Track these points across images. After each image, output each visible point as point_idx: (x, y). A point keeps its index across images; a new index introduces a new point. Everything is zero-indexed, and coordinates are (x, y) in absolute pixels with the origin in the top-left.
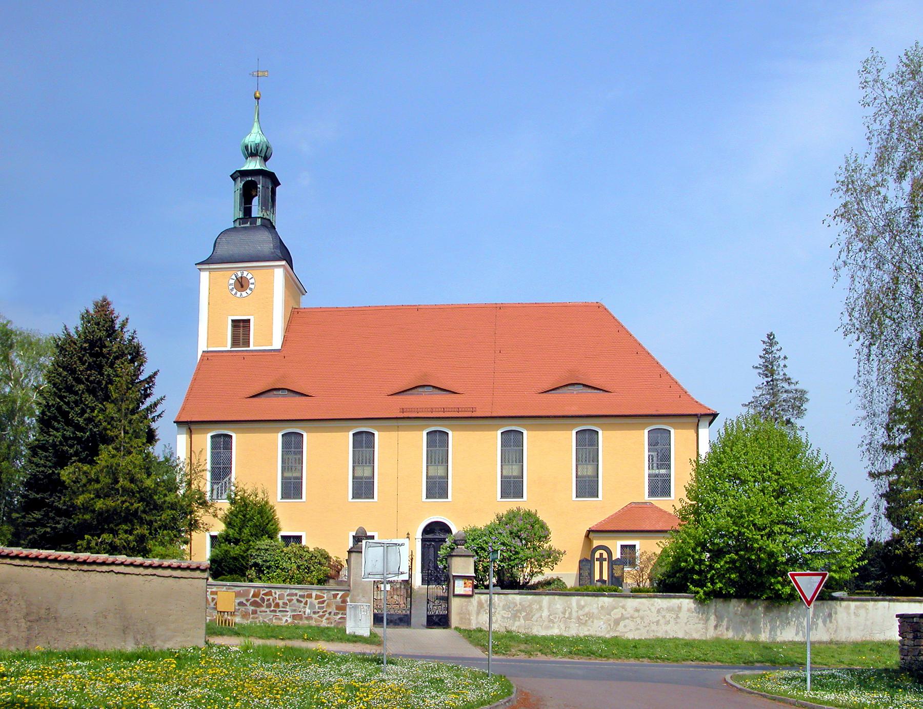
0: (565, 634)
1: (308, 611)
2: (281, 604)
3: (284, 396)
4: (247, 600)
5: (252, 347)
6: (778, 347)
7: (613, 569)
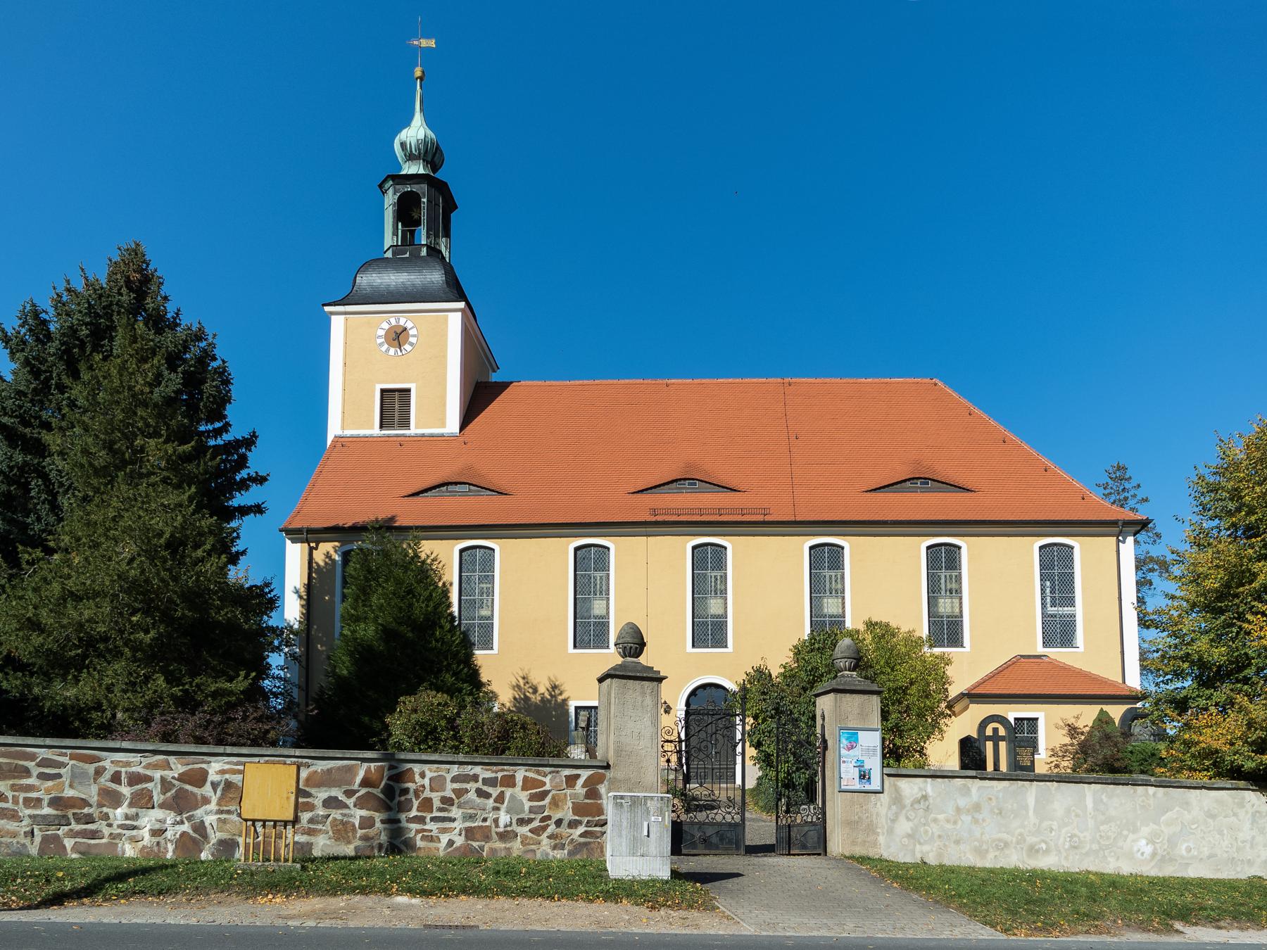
0: (979, 864)
1: (504, 818)
2: (437, 803)
3: (464, 494)
4: (349, 793)
5: (414, 430)
6: (1134, 482)
7: (1016, 754)
